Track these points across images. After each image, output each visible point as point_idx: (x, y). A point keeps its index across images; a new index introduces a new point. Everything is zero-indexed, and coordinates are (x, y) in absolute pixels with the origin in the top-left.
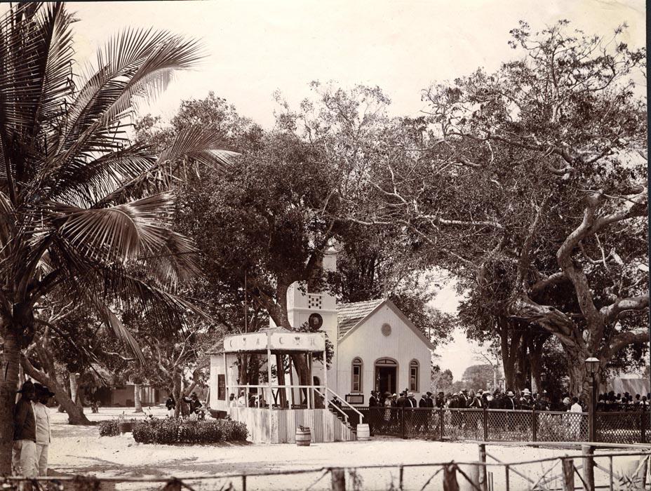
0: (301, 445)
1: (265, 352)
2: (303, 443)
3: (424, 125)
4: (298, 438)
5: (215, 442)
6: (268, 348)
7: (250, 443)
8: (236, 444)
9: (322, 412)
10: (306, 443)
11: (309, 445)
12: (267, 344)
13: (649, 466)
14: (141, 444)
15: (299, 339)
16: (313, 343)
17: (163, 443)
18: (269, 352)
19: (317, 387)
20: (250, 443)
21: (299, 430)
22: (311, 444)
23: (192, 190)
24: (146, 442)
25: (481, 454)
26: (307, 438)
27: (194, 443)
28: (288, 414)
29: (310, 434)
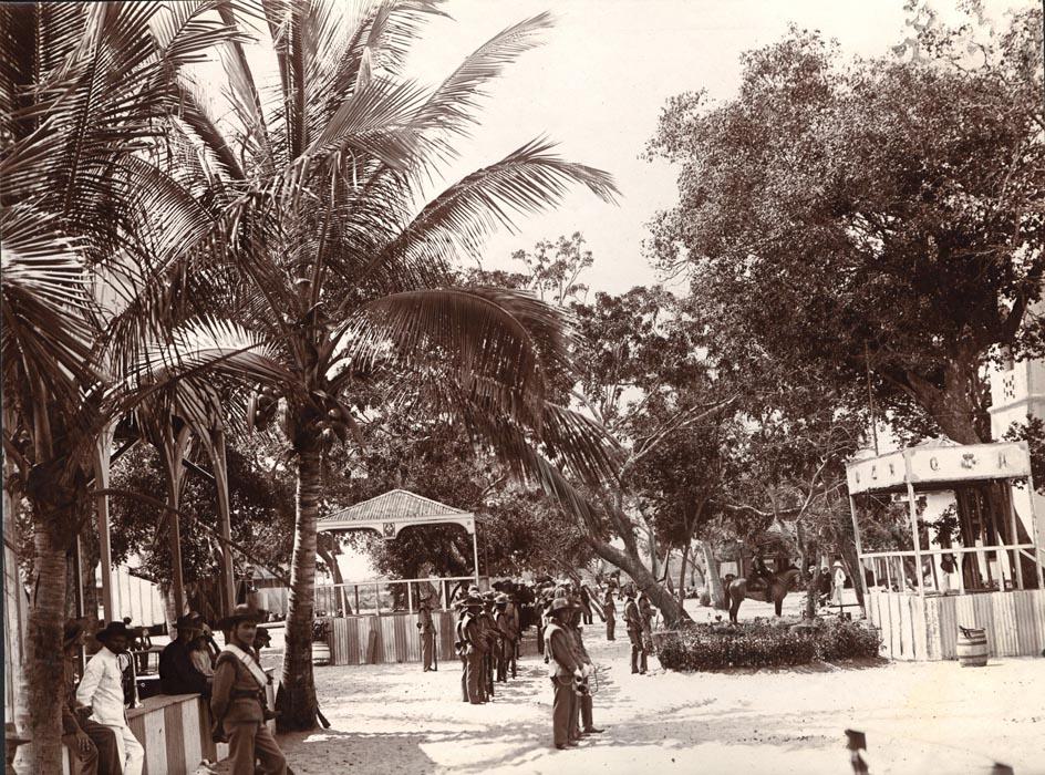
0: (967, 665)
1: (902, 489)
2: (971, 661)
3: (787, 78)
4: (961, 651)
5: (802, 663)
6: (908, 481)
7: (885, 661)
8: (847, 666)
9: (1032, 597)
10: (978, 661)
11: (984, 664)
12: (904, 473)
13: (690, 758)
14: (669, 671)
15: (971, 457)
16: (1002, 462)
17: (704, 669)
18: (911, 489)
19: (1027, 546)
20: (885, 661)
21: (961, 635)
22: (990, 662)
23: (728, 241)
24: (677, 669)
25: (701, 702)
26: (978, 650)
27: (760, 667)
28: (958, 604)
29: (985, 642)
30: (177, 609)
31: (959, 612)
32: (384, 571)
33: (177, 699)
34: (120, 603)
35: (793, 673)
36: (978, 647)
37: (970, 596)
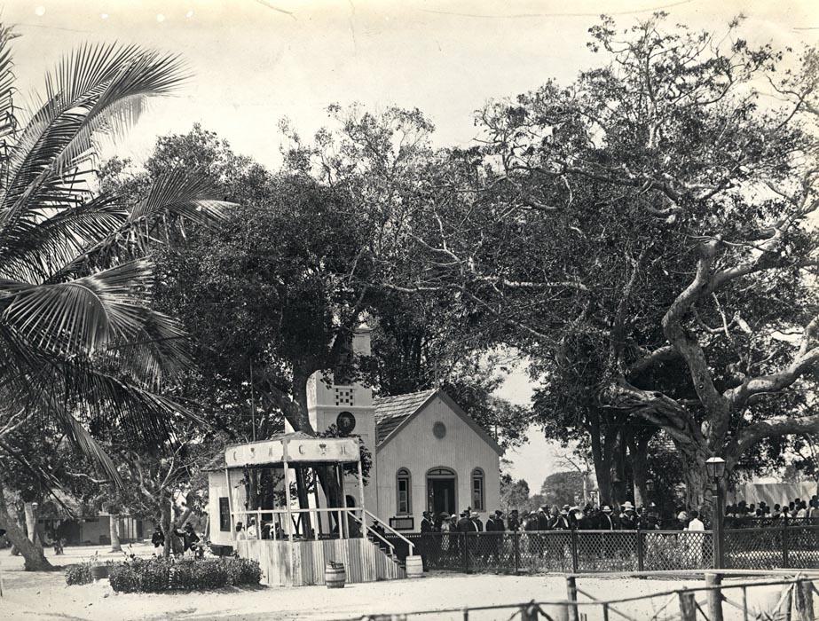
0: (332, 587)
2: (336, 584)
6: (285, 461)
7: (265, 587)
8: (247, 589)
9: (359, 543)
10: (338, 584)
11: (343, 587)
14: (121, 593)
16: (343, 451)
18: (286, 466)
20: (265, 587)
26: (340, 577)
28: (314, 547)
29: (344, 572)
30: (295, 422)
31: (314, 552)
32: (564, 437)
33: (136, 96)
34: (401, 519)
35: (215, 594)
36: (340, 575)
37: (322, 542)
